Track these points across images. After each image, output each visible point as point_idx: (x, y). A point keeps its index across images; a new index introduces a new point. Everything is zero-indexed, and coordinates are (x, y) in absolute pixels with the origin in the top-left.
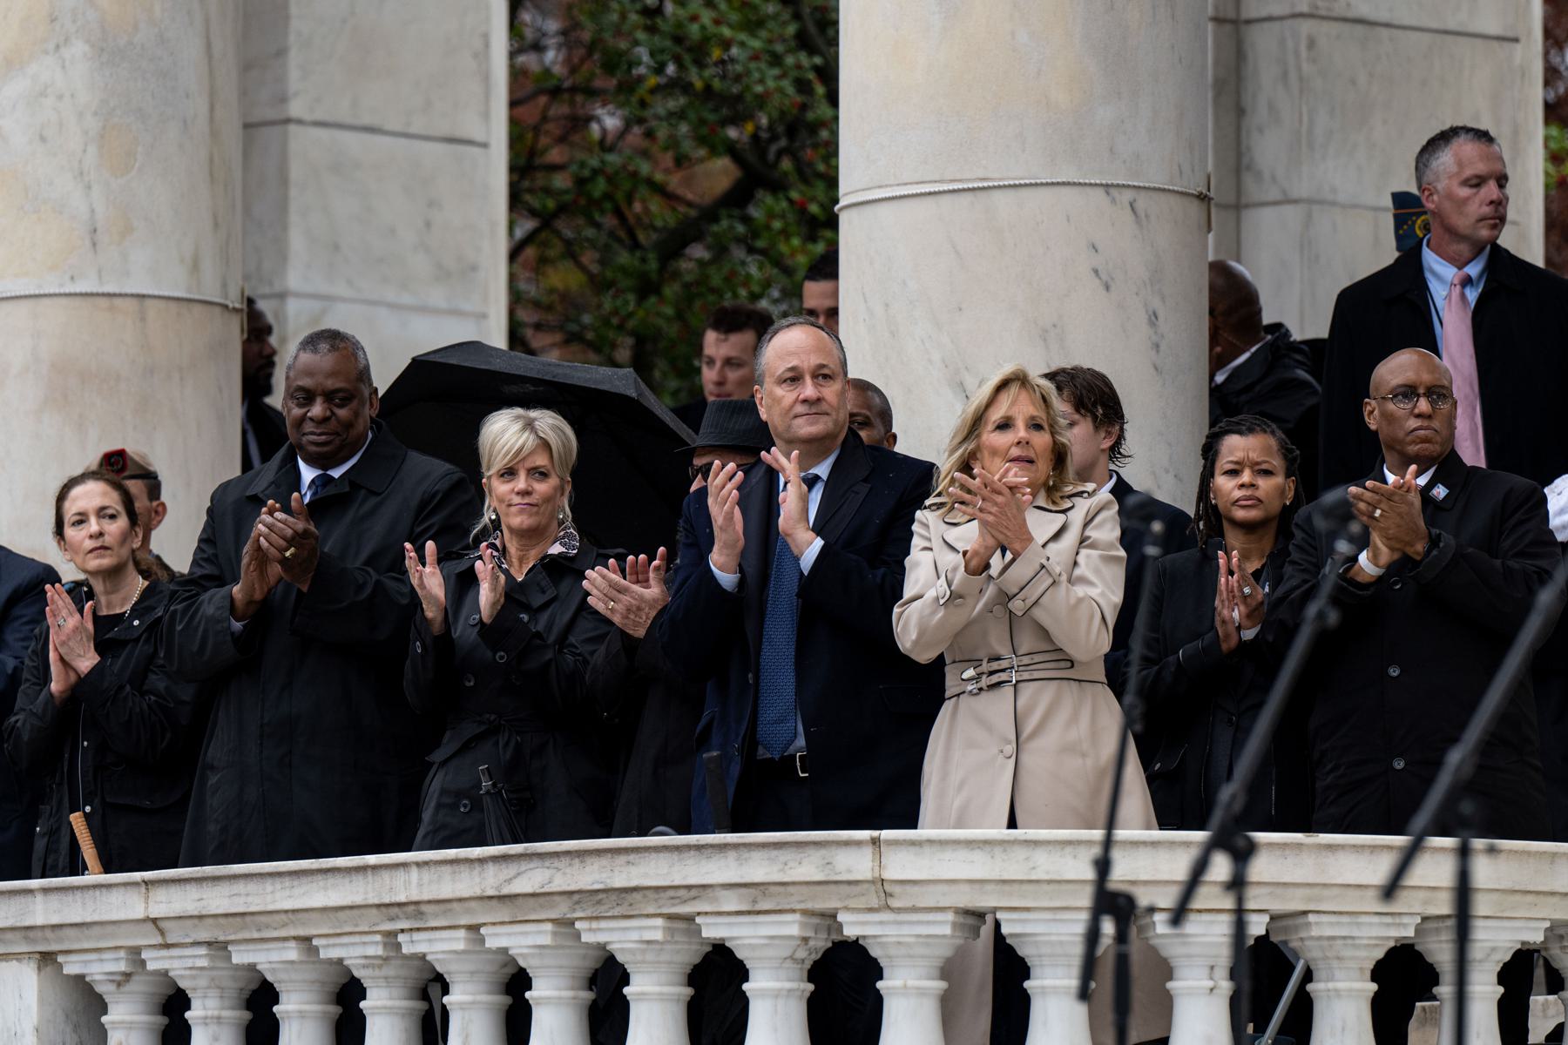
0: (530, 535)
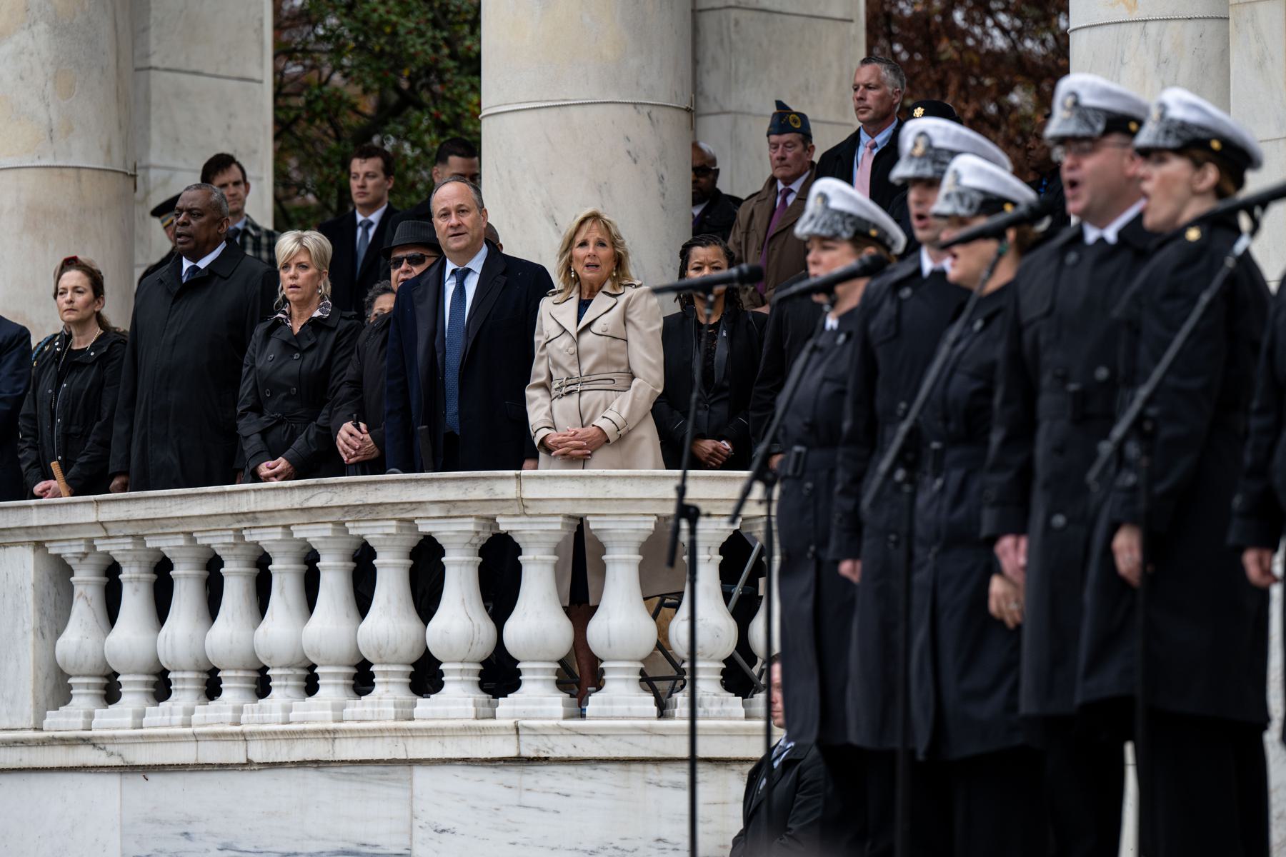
0: (304, 303)
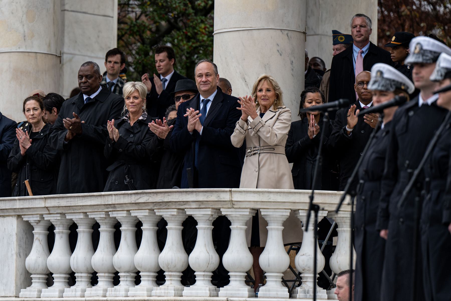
0: (135, 113)
